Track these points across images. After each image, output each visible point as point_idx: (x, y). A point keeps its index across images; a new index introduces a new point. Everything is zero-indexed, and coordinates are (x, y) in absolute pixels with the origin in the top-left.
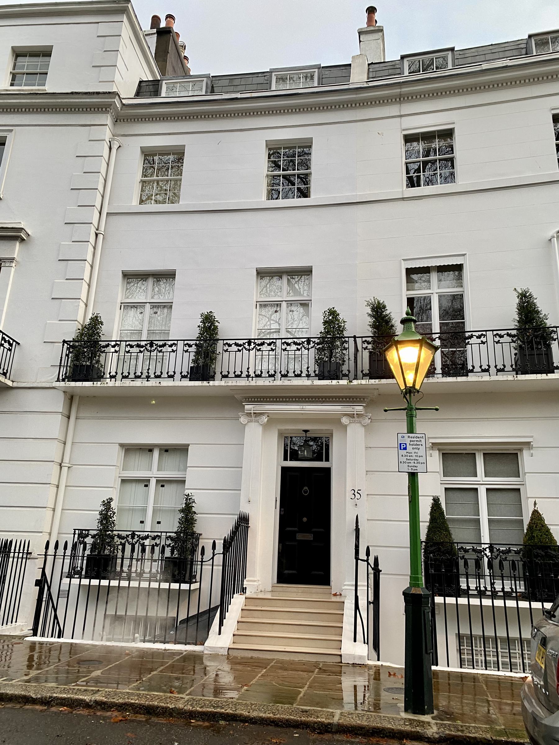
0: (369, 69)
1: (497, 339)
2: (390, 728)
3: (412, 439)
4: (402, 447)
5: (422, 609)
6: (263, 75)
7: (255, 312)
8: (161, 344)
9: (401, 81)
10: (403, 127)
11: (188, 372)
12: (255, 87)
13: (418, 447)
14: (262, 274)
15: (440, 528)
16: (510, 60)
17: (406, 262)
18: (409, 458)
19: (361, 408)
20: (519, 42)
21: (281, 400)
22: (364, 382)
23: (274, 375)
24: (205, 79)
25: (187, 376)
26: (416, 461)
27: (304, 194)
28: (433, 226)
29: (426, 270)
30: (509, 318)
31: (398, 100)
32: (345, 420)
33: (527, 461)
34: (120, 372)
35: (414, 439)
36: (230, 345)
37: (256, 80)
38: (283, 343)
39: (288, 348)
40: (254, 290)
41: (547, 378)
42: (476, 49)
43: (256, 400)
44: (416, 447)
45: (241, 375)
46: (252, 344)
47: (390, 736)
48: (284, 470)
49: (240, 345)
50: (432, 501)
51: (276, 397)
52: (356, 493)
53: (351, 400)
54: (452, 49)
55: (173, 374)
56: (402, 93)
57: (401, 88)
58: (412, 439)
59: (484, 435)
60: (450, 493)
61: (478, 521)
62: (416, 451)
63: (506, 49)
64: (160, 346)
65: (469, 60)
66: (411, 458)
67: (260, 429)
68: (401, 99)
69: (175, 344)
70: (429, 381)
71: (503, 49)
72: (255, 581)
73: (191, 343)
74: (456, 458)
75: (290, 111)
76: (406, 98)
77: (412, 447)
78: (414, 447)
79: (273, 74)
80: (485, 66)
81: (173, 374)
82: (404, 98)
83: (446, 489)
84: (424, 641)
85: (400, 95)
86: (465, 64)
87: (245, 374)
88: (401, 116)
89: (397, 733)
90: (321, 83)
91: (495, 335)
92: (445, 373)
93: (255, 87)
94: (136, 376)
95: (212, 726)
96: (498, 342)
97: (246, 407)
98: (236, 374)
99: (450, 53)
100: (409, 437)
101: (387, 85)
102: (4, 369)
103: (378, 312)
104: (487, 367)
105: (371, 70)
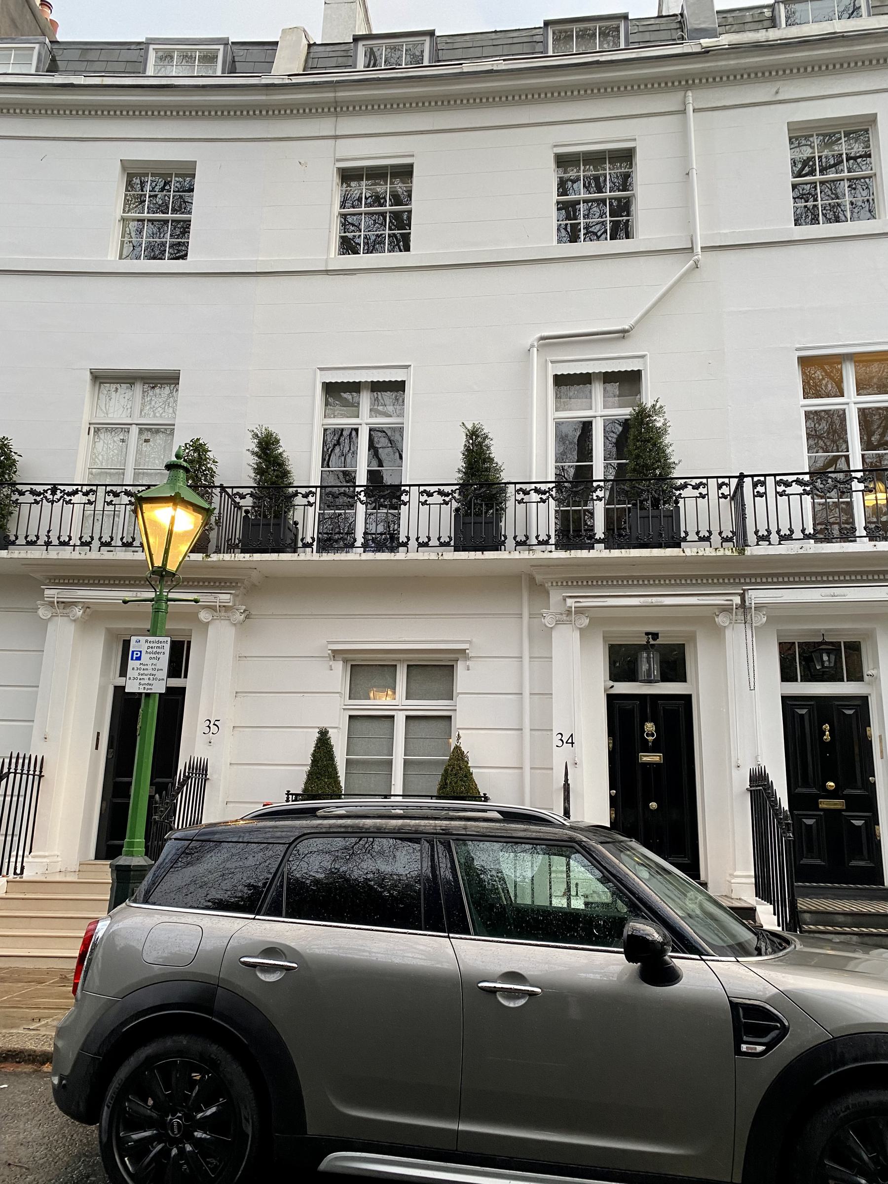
0: (308, 53)
1: (520, 496)
2: (31, 1050)
3: (151, 645)
4: (135, 656)
5: (131, 886)
6: (139, 47)
7: (85, 440)
8: (70, 490)
9: (335, 79)
10: (338, 156)
11: (450, 538)
12: (121, 67)
13: (158, 656)
14: (100, 378)
15: (320, 773)
16: (504, 60)
17: (323, 372)
18: (142, 672)
19: (228, 596)
20: (534, 32)
21: (107, 582)
22: (227, 557)
23: (90, 543)
24: (37, 46)
25: (449, 542)
26: (151, 677)
27: (180, 253)
28: (373, 319)
29: (355, 387)
30: (449, 467)
31: (332, 110)
32: (204, 616)
33: (463, 677)
34: (96, 537)
35: (153, 645)
36: (788, 484)
37: (126, 55)
38: (421, 493)
39: (116, 500)
40: (87, 406)
41: (483, 557)
42: (472, 37)
43: (66, 581)
44: (155, 656)
45: (36, 542)
46: (830, 481)
47: (29, 1060)
48: (612, 699)
49: (39, 494)
50: (318, 735)
51: (99, 578)
52: (211, 725)
53: (217, 584)
54: (431, 33)
55: (89, 539)
56: (338, 99)
57: (335, 91)
58: (153, 645)
59: (403, 639)
60: (414, 724)
61: (390, 763)
62: (155, 661)
63: (515, 40)
64: (69, 494)
65: (459, 54)
66: (146, 672)
67: (577, 634)
68: (337, 109)
69: (94, 491)
70: (321, 559)
71: (510, 41)
72: (45, 857)
73: (245, 491)
74: (366, 670)
75: (150, 113)
76: (345, 109)
77: (150, 656)
78: (152, 656)
79: (151, 47)
80: (467, 67)
81: (89, 539)
82: (342, 108)
83: (350, 717)
84: (539, 943)
85: (336, 102)
86: (451, 60)
87: (43, 539)
88: (336, 137)
89: (40, 1056)
90: (231, 68)
91: (778, 483)
92: (610, 542)
93: (121, 67)
94: (28, 542)
95: (35, 1071)
96: (424, 503)
97: (47, 592)
98: (442, 540)
99: (428, 39)
100: (147, 641)
101: (314, 83)
102: (803, 531)
103: (267, 449)
104: (707, 534)
105: (311, 55)
